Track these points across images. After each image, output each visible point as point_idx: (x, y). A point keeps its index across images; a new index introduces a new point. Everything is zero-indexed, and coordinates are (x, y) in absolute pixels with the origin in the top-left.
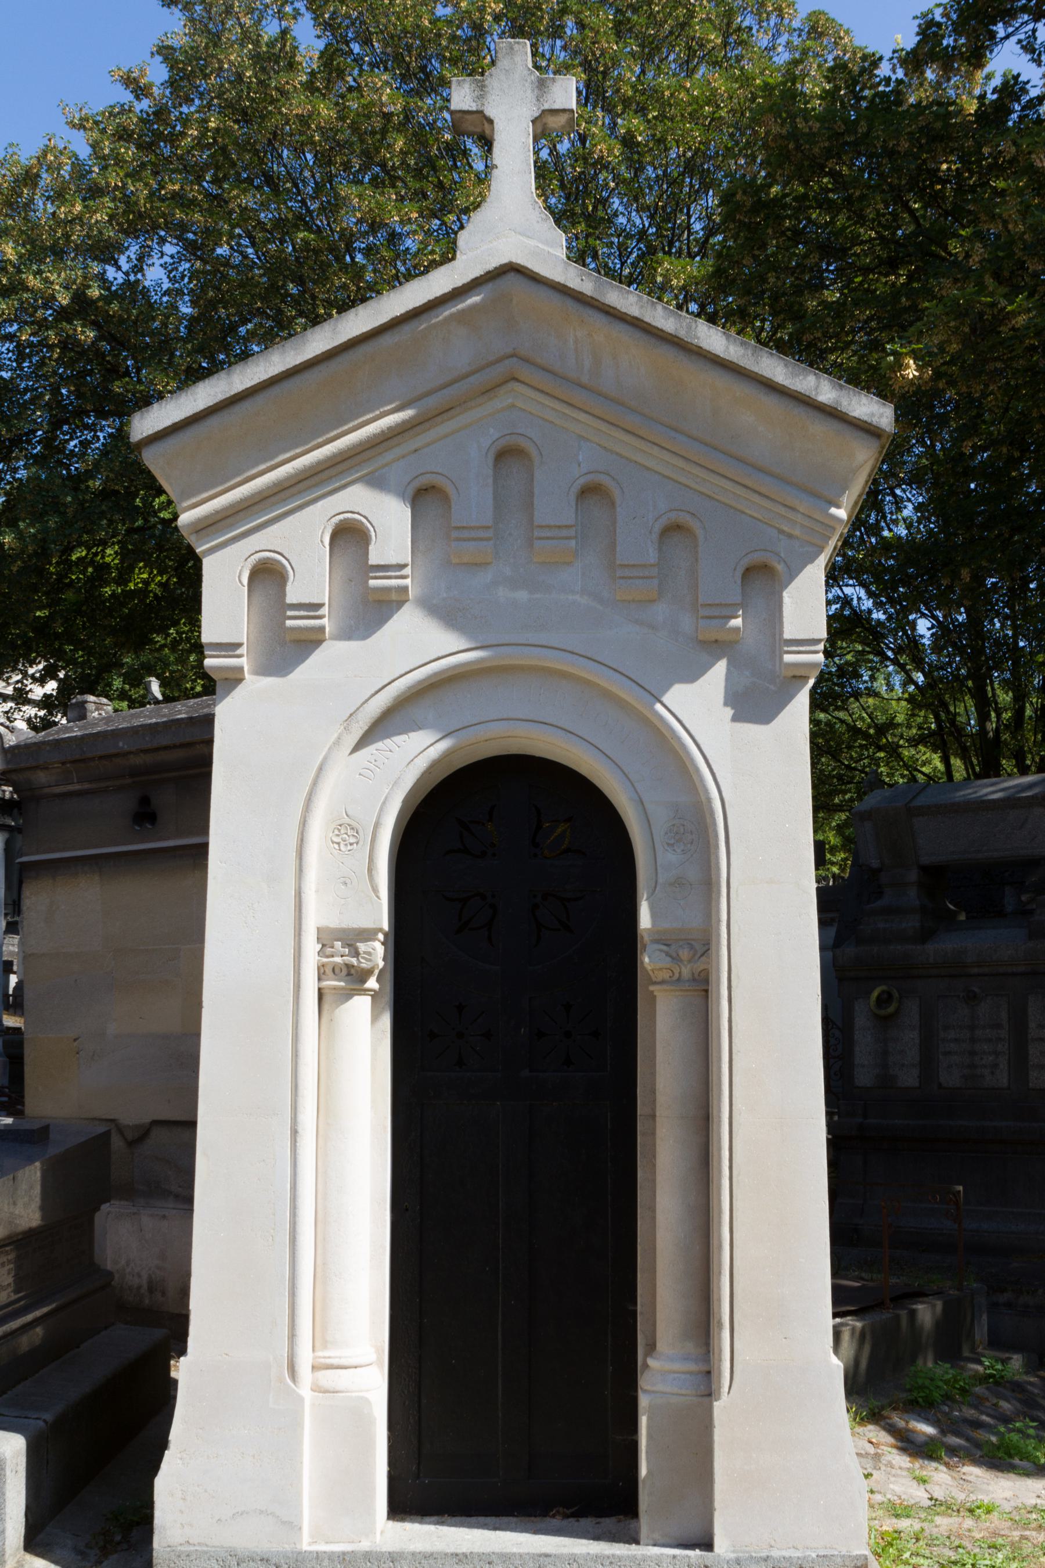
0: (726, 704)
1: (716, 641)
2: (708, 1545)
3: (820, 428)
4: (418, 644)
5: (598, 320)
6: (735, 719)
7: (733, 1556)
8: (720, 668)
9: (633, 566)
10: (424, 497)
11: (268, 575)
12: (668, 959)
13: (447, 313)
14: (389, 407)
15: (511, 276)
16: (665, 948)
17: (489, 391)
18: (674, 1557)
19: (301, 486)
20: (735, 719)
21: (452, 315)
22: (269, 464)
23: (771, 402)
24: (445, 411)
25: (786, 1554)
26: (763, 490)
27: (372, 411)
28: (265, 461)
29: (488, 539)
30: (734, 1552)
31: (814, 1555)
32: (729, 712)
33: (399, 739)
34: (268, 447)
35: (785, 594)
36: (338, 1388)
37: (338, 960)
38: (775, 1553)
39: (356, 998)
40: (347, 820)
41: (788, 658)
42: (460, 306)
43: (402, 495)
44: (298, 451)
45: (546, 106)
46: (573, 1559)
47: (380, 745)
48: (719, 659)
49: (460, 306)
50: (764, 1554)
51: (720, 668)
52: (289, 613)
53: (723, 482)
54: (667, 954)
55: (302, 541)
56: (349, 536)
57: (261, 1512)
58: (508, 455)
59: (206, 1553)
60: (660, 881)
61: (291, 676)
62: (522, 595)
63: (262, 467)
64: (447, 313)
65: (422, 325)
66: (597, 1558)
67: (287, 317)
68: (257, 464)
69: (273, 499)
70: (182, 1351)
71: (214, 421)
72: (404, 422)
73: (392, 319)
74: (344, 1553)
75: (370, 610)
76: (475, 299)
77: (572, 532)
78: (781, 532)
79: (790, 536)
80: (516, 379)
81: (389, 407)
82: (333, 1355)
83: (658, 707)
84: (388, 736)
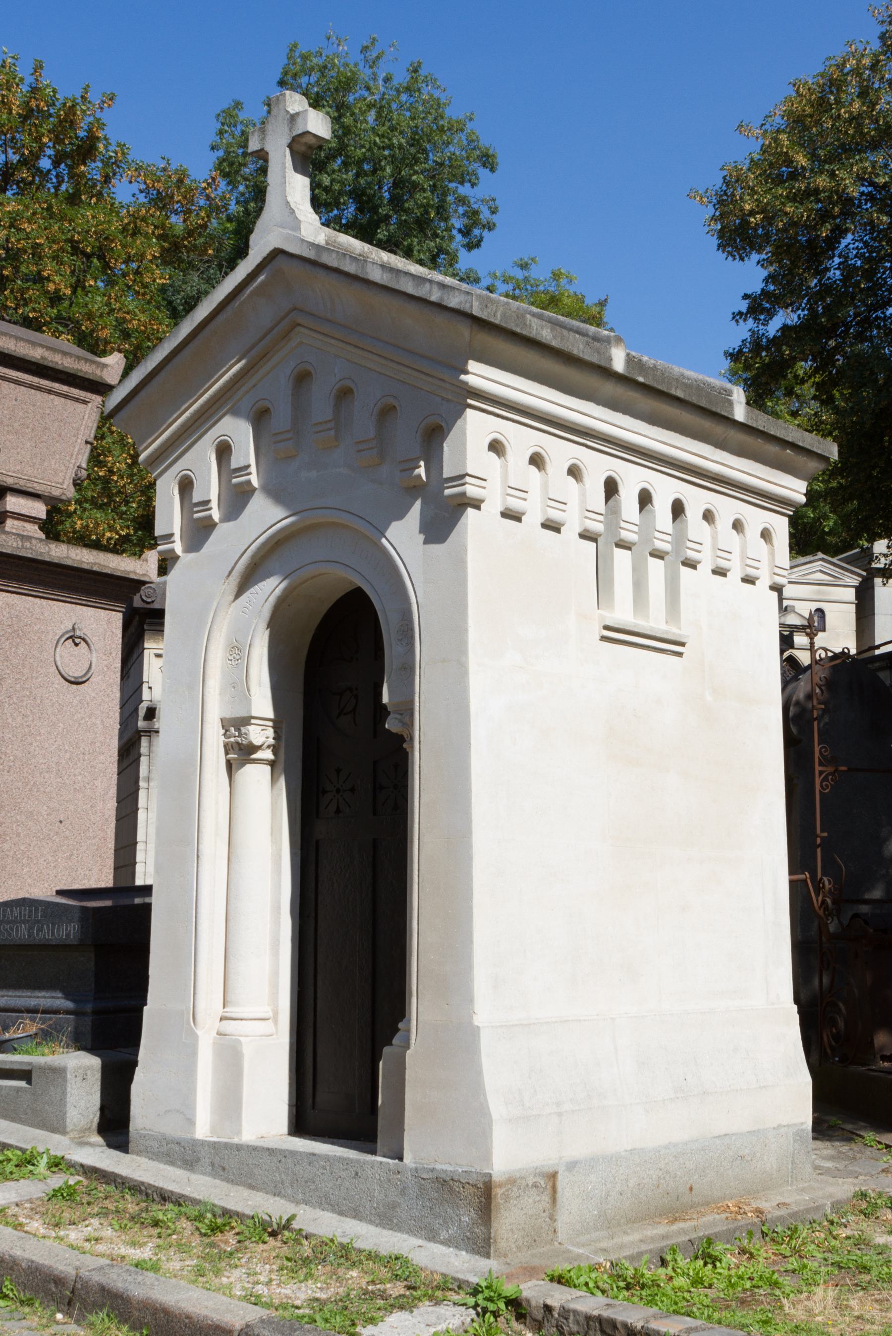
0: (420, 532)
1: (415, 487)
2: (401, 1159)
3: (440, 319)
4: (265, 517)
5: (321, 273)
6: (426, 542)
7: (413, 1165)
8: (417, 506)
9: (363, 441)
10: (260, 419)
11: (186, 486)
12: (401, 724)
13: (248, 292)
14: (232, 361)
15: (280, 258)
16: (399, 716)
17: (286, 335)
18: (381, 1163)
19: (197, 424)
20: (426, 542)
21: (251, 292)
22: (178, 413)
23: (411, 307)
24: (264, 356)
25: (444, 1167)
26: (424, 370)
27: (224, 366)
28: (176, 411)
29: (290, 439)
30: (415, 1163)
31: (460, 1170)
32: (422, 537)
33: (261, 584)
34: (176, 403)
35: (445, 445)
36: (227, 1032)
37: (232, 740)
38: (439, 1167)
39: (248, 765)
40: (236, 644)
41: (447, 492)
42: (255, 285)
43: (247, 418)
44: (191, 401)
45: (295, 134)
46: (327, 1158)
47: (252, 590)
48: (416, 500)
49: (255, 285)
50: (431, 1167)
51: (417, 506)
52: (195, 509)
53: (409, 371)
54: (400, 721)
55: (201, 461)
56: (224, 451)
57: (178, 1111)
58: (302, 378)
59: (152, 1135)
60: (394, 667)
61: (202, 551)
62: (314, 474)
63: (175, 416)
64: (248, 292)
65: (236, 303)
66: (341, 1159)
67: (63, 333)
68: (172, 415)
69: (185, 435)
70: (146, 1004)
71: (143, 394)
72: (241, 369)
73: (219, 304)
74: (215, 1143)
75: (237, 498)
76: (262, 278)
77: (329, 426)
78: (443, 399)
79: (448, 400)
80: (299, 325)
81: (232, 361)
82: (232, 1011)
83: (384, 541)
84: (256, 584)
